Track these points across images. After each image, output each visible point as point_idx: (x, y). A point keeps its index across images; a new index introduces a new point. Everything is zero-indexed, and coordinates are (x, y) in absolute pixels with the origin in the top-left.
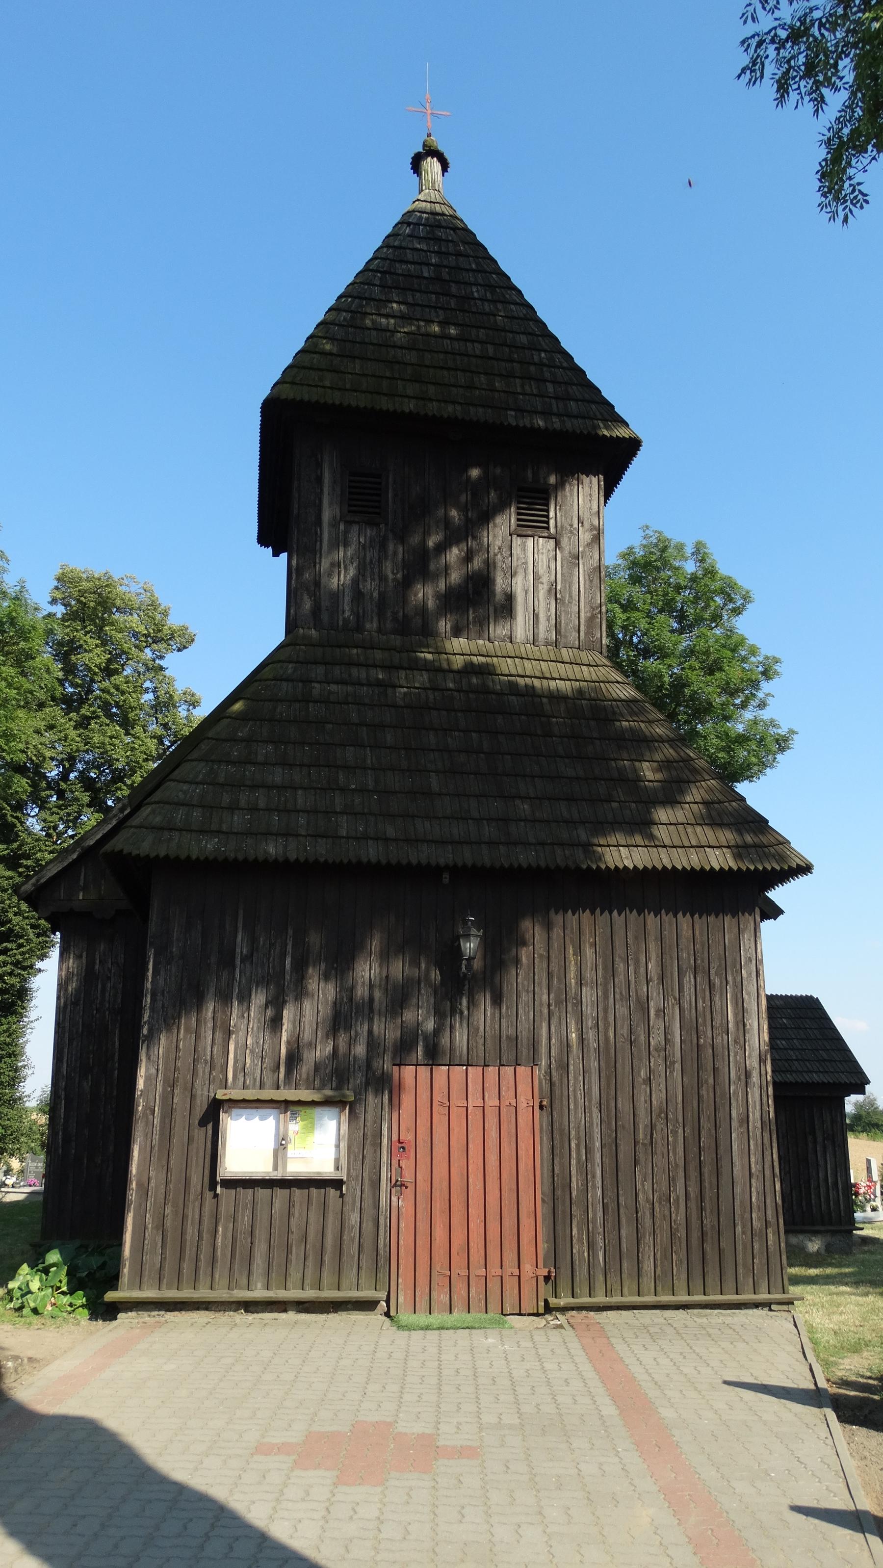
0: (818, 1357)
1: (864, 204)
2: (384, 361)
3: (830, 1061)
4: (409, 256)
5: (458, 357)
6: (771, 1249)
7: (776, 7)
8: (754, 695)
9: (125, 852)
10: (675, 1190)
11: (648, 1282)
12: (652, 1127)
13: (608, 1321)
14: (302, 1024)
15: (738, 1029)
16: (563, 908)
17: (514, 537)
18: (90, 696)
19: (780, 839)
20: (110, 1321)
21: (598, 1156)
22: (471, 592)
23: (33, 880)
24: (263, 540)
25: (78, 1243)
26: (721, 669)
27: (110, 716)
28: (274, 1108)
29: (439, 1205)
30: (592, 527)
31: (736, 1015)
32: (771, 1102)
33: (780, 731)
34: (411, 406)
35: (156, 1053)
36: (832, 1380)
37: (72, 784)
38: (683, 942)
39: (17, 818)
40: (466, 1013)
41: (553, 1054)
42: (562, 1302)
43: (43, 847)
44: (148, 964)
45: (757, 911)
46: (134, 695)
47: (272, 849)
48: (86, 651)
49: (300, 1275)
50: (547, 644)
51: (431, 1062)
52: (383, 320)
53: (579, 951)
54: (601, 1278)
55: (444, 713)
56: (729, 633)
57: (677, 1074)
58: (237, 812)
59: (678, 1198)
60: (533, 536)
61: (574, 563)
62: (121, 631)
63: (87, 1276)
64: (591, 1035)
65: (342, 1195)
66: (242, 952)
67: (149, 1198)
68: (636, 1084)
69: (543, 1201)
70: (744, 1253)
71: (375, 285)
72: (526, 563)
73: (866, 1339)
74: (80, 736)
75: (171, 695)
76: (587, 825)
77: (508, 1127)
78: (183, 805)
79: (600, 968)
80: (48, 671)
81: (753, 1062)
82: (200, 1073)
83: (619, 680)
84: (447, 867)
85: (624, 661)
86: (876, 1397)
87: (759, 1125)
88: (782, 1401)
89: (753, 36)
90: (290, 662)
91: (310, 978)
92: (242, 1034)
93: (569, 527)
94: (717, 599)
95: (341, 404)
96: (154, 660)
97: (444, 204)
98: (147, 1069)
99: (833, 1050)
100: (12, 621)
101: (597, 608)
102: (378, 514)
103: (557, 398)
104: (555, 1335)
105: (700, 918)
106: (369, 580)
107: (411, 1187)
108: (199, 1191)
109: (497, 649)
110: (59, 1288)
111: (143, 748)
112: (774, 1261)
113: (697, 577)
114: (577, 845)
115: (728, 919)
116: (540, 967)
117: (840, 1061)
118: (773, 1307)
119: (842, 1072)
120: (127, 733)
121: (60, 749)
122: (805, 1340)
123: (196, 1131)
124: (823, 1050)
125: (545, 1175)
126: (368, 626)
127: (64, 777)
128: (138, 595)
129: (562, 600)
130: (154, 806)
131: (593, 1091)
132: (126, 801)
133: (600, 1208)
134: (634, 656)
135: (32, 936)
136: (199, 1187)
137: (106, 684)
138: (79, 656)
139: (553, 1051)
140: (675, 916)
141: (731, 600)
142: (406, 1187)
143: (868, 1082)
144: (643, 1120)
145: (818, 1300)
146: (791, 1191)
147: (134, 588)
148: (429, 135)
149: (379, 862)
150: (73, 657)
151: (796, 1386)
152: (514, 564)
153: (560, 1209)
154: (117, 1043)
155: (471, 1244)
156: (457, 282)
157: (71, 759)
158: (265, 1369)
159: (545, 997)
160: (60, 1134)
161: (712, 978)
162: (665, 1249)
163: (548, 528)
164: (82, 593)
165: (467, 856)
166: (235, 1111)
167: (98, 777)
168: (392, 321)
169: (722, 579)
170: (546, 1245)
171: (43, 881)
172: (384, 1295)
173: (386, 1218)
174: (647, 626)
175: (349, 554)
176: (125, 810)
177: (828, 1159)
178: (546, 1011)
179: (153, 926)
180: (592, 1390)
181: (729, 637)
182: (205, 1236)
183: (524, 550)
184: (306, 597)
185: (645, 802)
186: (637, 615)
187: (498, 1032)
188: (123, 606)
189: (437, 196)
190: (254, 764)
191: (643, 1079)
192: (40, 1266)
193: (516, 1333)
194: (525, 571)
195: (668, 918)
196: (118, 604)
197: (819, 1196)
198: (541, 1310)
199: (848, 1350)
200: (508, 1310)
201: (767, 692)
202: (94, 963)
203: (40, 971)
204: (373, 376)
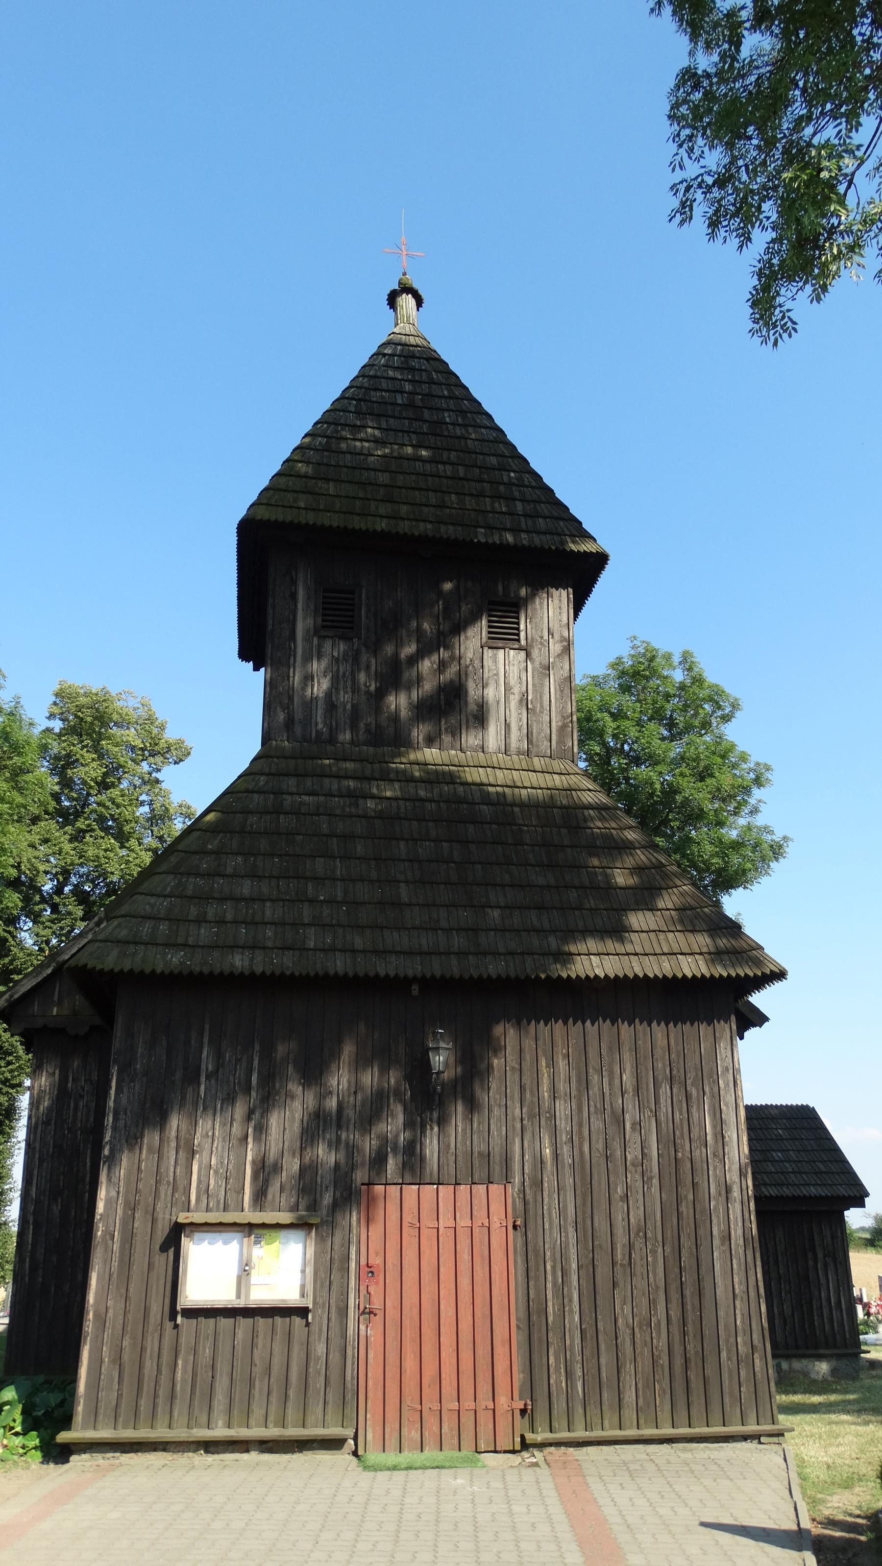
0: (804, 1494)
1: (793, 332)
2: (357, 483)
4: (384, 384)
5: (430, 478)
6: (759, 1375)
7: (701, 156)
8: (746, 801)
9: (89, 966)
10: (656, 1314)
11: (630, 1414)
12: (631, 1246)
13: (587, 1458)
14: (268, 1143)
15: (716, 1142)
16: (547, 1018)
17: (486, 649)
18: (86, 810)
19: (754, 944)
20: (63, 1463)
21: (575, 1278)
22: (442, 703)
23: (7, 996)
24: (244, 655)
25: (41, 1379)
26: (712, 776)
27: (106, 830)
28: (238, 1231)
29: (410, 1333)
30: (563, 639)
31: (714, 1127)
32: (753, 1218)
33: (774, 837)
34: (383, 525)
35: (117, 1174)
36: (818, 1519)
37: (65, 898)
38: (658, 1052)
39: (9, 932)
41: (526, 1171)
42: (539, 1437)
44: (111, 1081)
47: (239, 962)
48: (82, 765)
49: (263, 1412)
50: (519, 753)
51: (401, 1181)
52: (358, 444)
53: (552, 1063)
54: (580, 1410)
55: (415, 823)
56: (718, 740)
57: (655, 1189)
58: (204, 925)
59: (659, 1321)
60: (504, 648)
61: (545, 674)
62: (117, 745)
63: (43, 1414)
64: (566, 1150)
65: (308, 1324)
66: (207, 1069)
67: (106, 1329)
69: (518, 1327)
70: (731, 1381)
71: (351, 412)
72: (497, 675)
73: (861, 1473)
74: (74, 849)
75: (166, 808)
76: (557, 933)
77: (480, 1248)
78: (149, 918)
79: (574, 1079)
80: (42, 786)
81: (733, 1176)
82: (163, 1196)
83: (591, 787)
84: (415, 978)
85: (616, 769)
86: (863, 1538)
87: (741, 1242)
88: (761, 1544)
89: (681, 182)
90: (262, 774)
91: (276, 1095)
92: (206, 1154)
93: (539, 639)
94: (706, 706)
95: (314, 524)
96: (150, 774)
97: (418, 336)
98: (107, 1191)
99: (830, 1161)
100: (6, 737)
101: (568, 717)
102: (352, 628)
103: (525, 516)
104: (529, 1475)
105: (675, 1026)
107: (380, 1315)
109: (469, 758)
110: (13, 1428)
111: (138, 861)
112: (763, 1388)
113: (685, 686)
114: (548, 955)
115: (703, 1027)
116: (513, 1079)
117: (838, 1173)
118: (763, 1439)
119: (841, 1185)
120: (122, 847)
122: (793, 1476)
123: (157, 1257)
124: (820, 1161)
125: (520, 1300)
126: (341, 738)
127: (59, 891)
128: (135, 709)
129: (534, 710)
130: (120, 920)
131: (569, 1209)
134: (626, 764)
137: (102, 798)
138: (75, 770)
139: (526, 1168)
140: (650, 1025)
141: (719, 707)
142: (375, 1315)
143: (867, 1195)
144: (621, 1239)
145: (816, 1430)
146: (793, 1311)
147: (132, 703)
148: (404, 274)
149: (346, 974)
151: (776, 1527)
152: (486, 676)
153: (536, 1336)
154: (88, 1164)
155: (443, 1376)
157: (66, 873)
158: (216, 1516)
159: (517, 1111)
160: (28, 1260)
161: (688, 1089)
163: (518, 640)
164: (79, 708)
165: (436, 968)
166: (197, 1235)
167: (92, 890)
168: (366, 444)
169: (709, 687)
171: (16, 996)
172: (350, 1432)
173: (354, 1348)
174: (637, 734)
176: (102, 923)
177: (830, 1277)
178: (518, 1126)
180: (558, 1535)
181: (719, 744)
182: (165, 1370)
183: (495, 661)
185: (616, 910)
186: (627, 723)
188: (120, 720)
189: (412, 329)
190: (223, 876)
191: (621, 1197)
193: (488, 1472)
195: (641, 1028)
196: (114, 719)
197: (821, 1316)
198: (518, 1447)
199: (839, 1486)
200: (482, 1447)
201: (759, 798)
202: (67, 1081)
204: (347, 497)
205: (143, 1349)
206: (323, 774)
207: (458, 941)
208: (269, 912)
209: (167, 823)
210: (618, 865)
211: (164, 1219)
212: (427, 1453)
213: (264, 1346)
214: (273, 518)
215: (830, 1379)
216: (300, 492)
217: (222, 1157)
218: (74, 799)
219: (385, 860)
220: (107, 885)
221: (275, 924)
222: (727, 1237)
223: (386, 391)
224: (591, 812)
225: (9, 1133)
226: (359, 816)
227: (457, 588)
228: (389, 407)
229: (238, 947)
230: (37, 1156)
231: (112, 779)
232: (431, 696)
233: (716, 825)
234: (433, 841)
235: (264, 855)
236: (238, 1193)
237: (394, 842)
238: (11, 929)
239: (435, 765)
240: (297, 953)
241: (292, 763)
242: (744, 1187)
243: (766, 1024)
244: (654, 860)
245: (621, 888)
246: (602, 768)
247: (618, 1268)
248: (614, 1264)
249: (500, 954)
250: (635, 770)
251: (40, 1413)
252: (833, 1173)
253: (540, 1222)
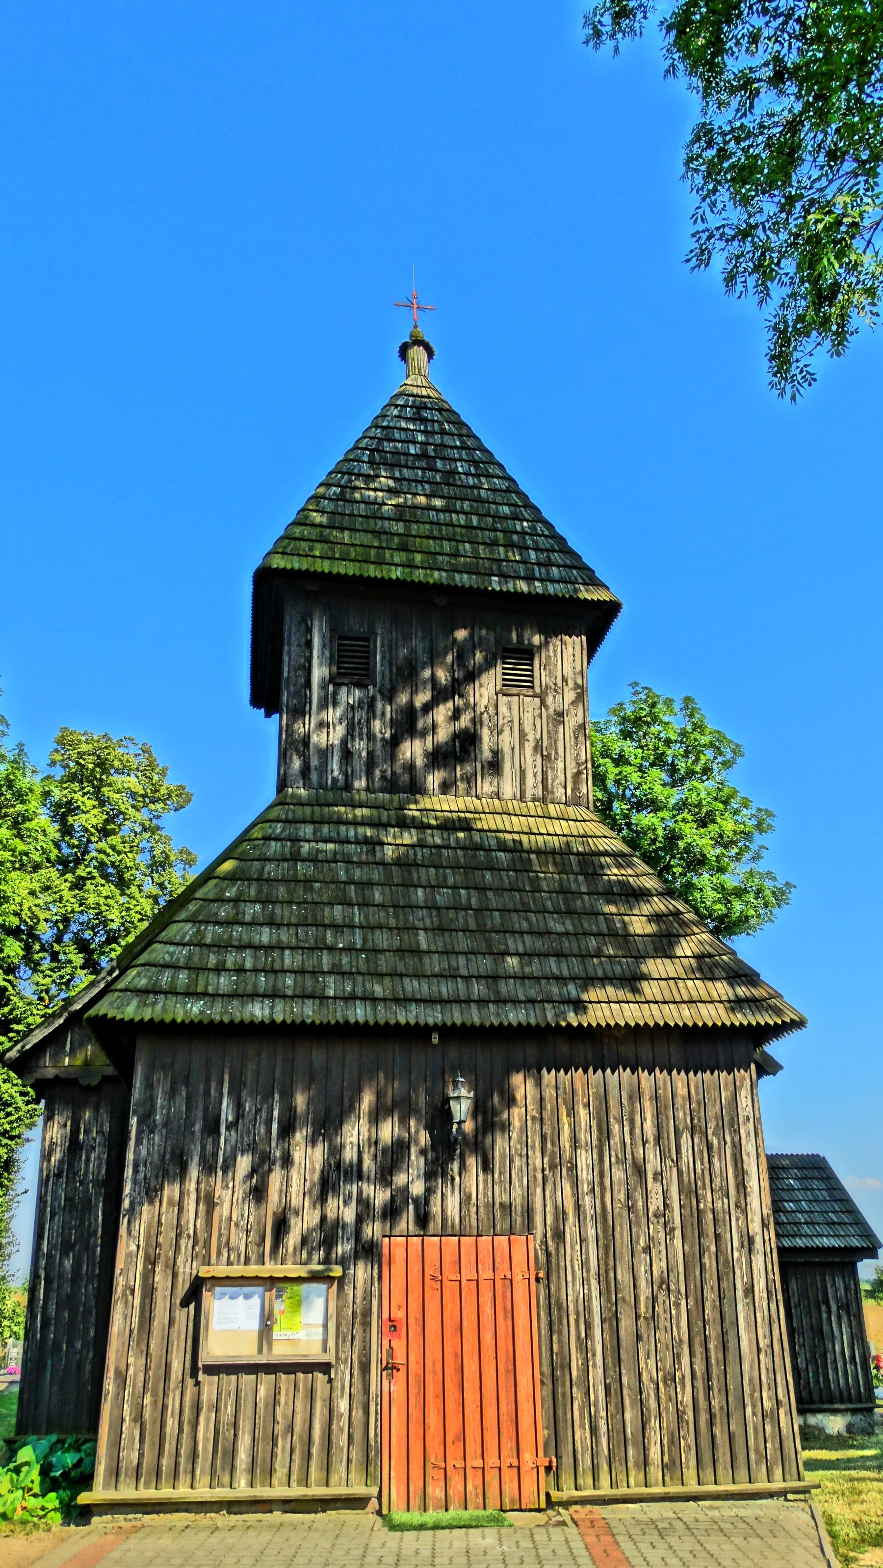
0: (836, 1551)
2: (371, 532)
3: (839, 1224)
4: (397, 435)
5: (444, 527)
6: (784, 1431)
9: (109, 1016)
10: (680, 1368)
12: (654, 1299)
15: (738, 1192)
17: (500, 696)
23: (18, 1047)
25: (54, 1438)
26: (714, 821)
27: (105, 876)
29: (432, 1389)
30: (577, 686)
31: (736, 1177)
33: (776, 883)
34: (399, 573)
38: (679, 1101)
39: (9, 981)
40: (457, 1179)
41: (549, 1222)
42: (568, 1492)
43: (35, 1012)
45: (753, 1066)
46: (130, 855)
47: (258, 1011)
48: (83, 812)
49: (286, 1470)
52: (372, 493)
54: (605, 1467)
55: (432, 870)
57: (678, 1241)
58: (223, 973)
59: (683, 1377)
60: (518, 695)
64: (587, 1200)
68: (636, 1253)
70: (756, 1439)
71: (363, 462)
72: (511, 721)
74: (75, 897)
81: (755, 1227)
82: (183, 1249)
87: (765, 1295)
90: (279, 821)
95: (330, 572)
96: (151, 820)
103: (539, 564)
106: (357, 740)
107: (403, 1369)
108: (180, 1378)
111: (138, 908)
121: (55, 910)
123: (178, 1312)
126: (357, 784)
127: (59, 940)
130: (139, 969)
132: (114, 963)
135: (21, 1104)
136: (180, 1374)
137: (102, 845)
141: (721, 754)
142: (398, 1370)
148: (416, 327)
149: (367, 1022)
150: (70, 819)
152: (500, 723)
156: (443, 459)
162: (672, 1434)
163: (532, 687)
164: (81, 755)
165: (456, 1016)
166: (218, 1290)
168: (380, 494)
170: (546, 1432)
171: (28, 1047)
172: (374, 1491)
175: (338, 715)
178: (539, 1176)
179: (137, 1093)
182: (186, 1427)
184: (295, 757)
186: (629, 769)
187: (490, 1200)
190: (242, 924)
192: (12, 1465)
193: (515, 1532)
194: (511, 729)
198: (543, 1505)
199: (870, 1544)
202: (78, 1132)
203: (28, 1140)
204: (361, 545)
205: (164, 1408)
206: (340, 822)
207: (478, 989)
208: (289, 959)
209: (168, 870)
210: (636, 912)
211: (184, 1273)
212: (430, 1512)
213: (286, 1403)
214: (289, 567)
215: (845, 1434)
217: (243, 1209)
218: (73, 846)
219: (403, 907)
220: (108, 932)
221: (295, 972)
222: (750, 1291)
223: (399, 441)
224: (608, 859)
225: (7, 1187)
226: (376, 863)
227: (472, 635)
228: (402, 457)
229: (258, 995)
230: (49, 1209)
231: (113, 826)
232: (447, 743)
233: (718, 871)
234: (450, 888)
235: (281, 903)
236: (259, 1245)
237: (412, 889)
238: (11, 977)
239: (451, 812)
240: (317, 1001)
241: (308, 810)
242: (767, 1238)
243: (780, 1072)
244: (671, 907)
245: (638, 936)
246: (604, 814)
248: (637, 1317)
249: (520, 1002)
250: (635, 818)
251: (58, 1474)
252: (845, 1224)
253: (562, 1275)
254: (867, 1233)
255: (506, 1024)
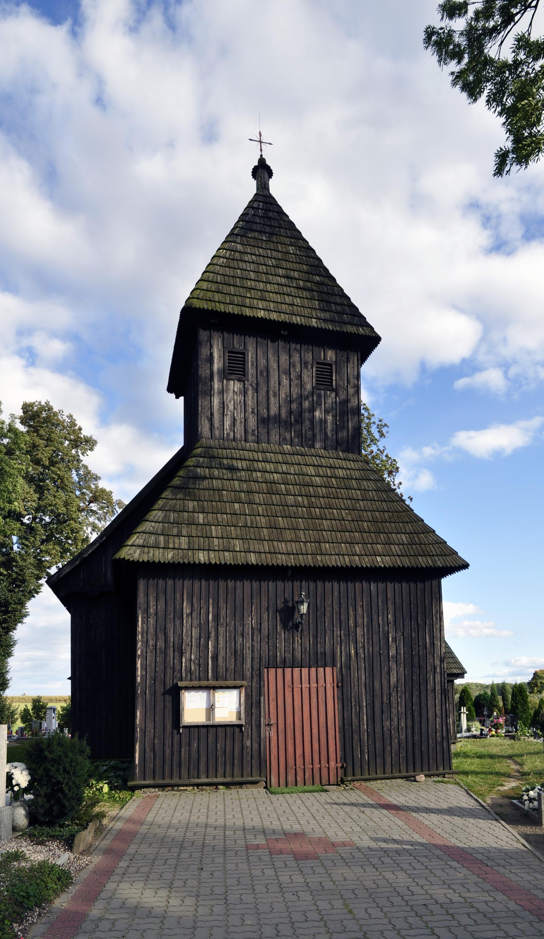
9: (126, 559)
31: (430, 639)
34: (262, 314)
53: (355, 610)
57: (402, 669)
64: (361, 651)
78: (153, 534)
107: (275, 726)
117: (453, 663)
133: (366, 733)
143: (466, 673)
149: (296, 565)
153: (347, 735)
163: (332, 386)
178: (339, 640)
200: (324, 783)
216: (215, 292)
247: (384, 705)
254: (462, 668)
255: (317, 566)
